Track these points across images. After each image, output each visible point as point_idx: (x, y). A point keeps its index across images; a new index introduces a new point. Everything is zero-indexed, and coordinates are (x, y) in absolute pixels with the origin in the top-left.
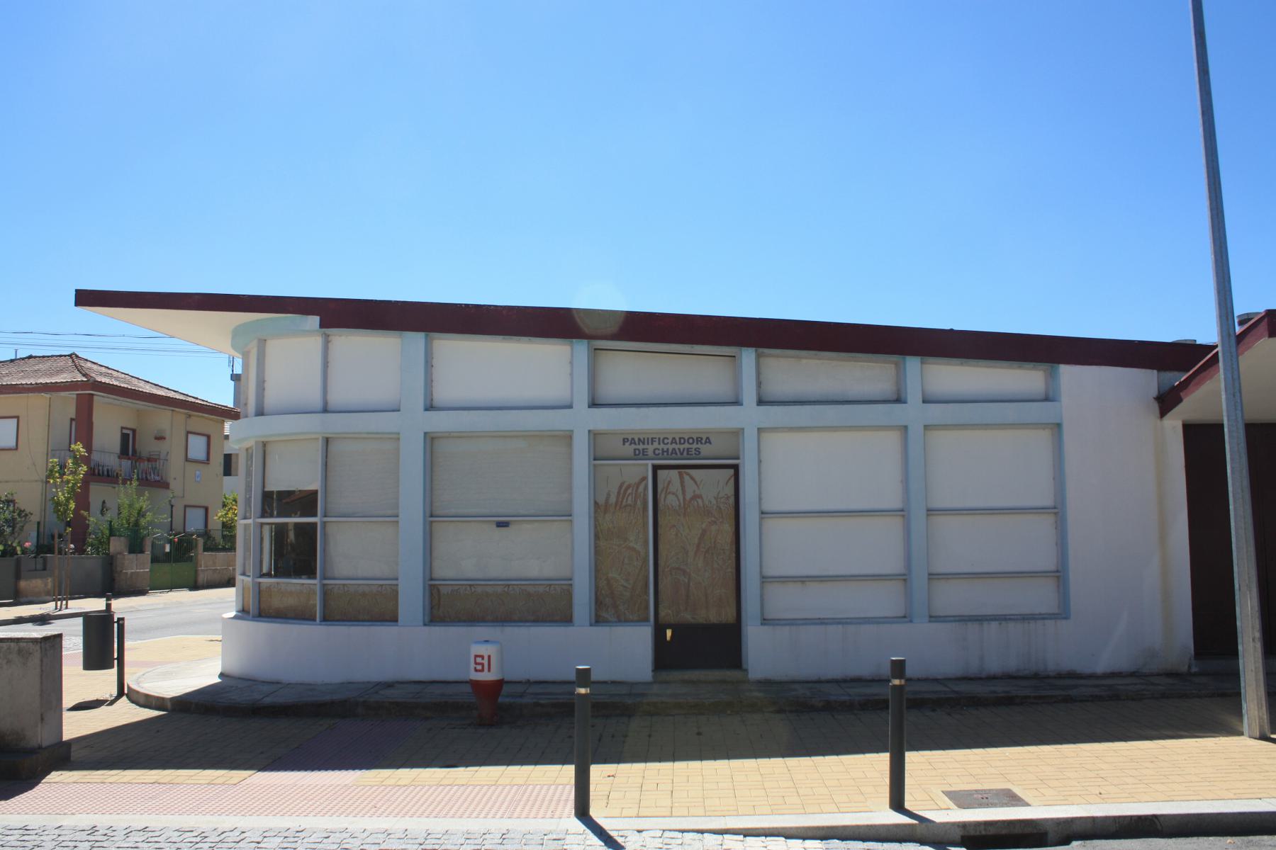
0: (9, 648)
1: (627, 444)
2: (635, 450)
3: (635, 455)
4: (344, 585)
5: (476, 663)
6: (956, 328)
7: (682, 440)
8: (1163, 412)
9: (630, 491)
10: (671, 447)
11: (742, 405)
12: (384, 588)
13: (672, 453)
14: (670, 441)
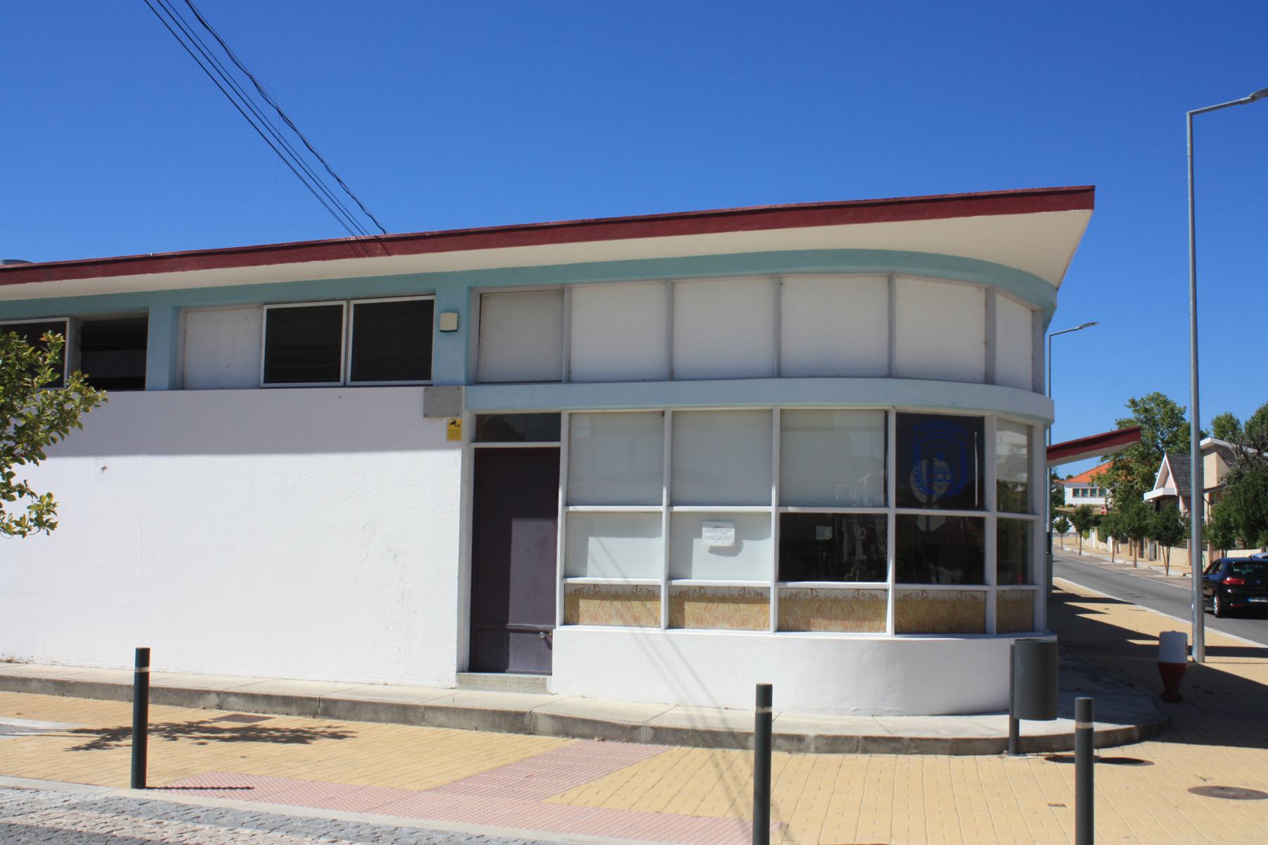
12: (861, 594)
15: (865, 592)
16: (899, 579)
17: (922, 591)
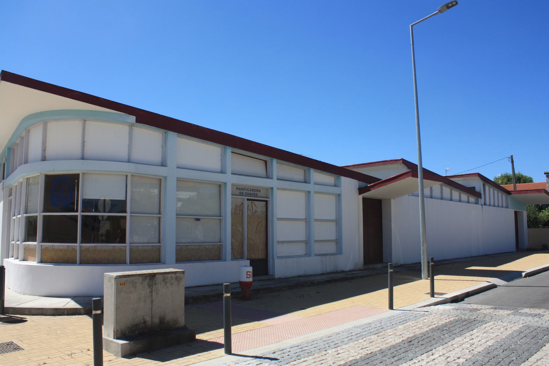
0: (171, 277)
1: (238, 189)
2: (240, 192)
3: (240, 194)
4: (137, 246)
5: (247, 275)
6: (322, 161)
7: (253, 190)
9: (238, 208)
10: (250, 192)
11: (167, 167)
12: (69, 248)
13: (250, 195)
14: (249, 190)
15: (117, 247)
16: (45, 239)
17: (53, 246)
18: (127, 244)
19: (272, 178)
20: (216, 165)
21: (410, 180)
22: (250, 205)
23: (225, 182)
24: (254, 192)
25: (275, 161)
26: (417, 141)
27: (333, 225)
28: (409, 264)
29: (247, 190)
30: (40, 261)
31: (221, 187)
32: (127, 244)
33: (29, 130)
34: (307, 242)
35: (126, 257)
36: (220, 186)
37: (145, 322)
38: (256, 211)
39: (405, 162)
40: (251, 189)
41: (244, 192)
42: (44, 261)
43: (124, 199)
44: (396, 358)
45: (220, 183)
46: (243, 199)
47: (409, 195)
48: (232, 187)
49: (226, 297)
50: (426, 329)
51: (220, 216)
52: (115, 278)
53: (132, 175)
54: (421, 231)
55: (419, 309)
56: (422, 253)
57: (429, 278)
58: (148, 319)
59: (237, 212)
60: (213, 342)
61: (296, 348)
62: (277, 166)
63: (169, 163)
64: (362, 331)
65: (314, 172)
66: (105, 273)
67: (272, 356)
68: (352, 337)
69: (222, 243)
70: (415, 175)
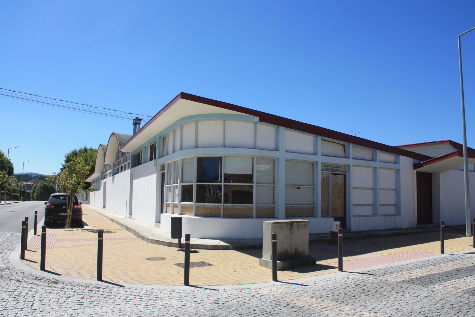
3: (327, 170)
4: (260, 206)
5: (337, 227)
6: (385, 144)
8: (414, 169)
16: (198, 201)
17: (233, 206)
18: (254, 204)
19: (349, 158)
20: (310, 149)
21: (456, 158)
22: (334, 178)
23: (317, 161)
24: (336, 168)
25: (351, 145)
26: (462, 117)
27: (371, 192)
28: (454, 226)
29: (332, 166)
30: (195, 215)
31: (313, 165)
32: (254, 204)
33: (183, 126)
34: (374, 206)
35: (253, 213)
36: (313, 164)
37: (287, 251)
38: (338, 182)
39: (452, 143)
40: (334, 166)
41: (330, 168)
42: (197, 215)
43: (251, 174)
44: (449, 277)
45: (313, 162)
46: (329, 173)
47: (455, 170)
48: (322, 164)
49: (340, 236)
50: (469, 265)
51: (313, 186)
52: (272, 224)
53: (257, 157)
54: (466, 199)
55: (464, 255)
56: (466, 216)
57: (472, 236)
58: (289, 249)
59: (325, 182)
60: (327, 266)
61: (382, 270)
62: (353, 150)
63: (280, 149)
64: (424, 264)
65: (380, 152)
66: (264, 221)
67: (369, 273)
68: (418, 267)
69: (315, 205)
70: (461, 154)
